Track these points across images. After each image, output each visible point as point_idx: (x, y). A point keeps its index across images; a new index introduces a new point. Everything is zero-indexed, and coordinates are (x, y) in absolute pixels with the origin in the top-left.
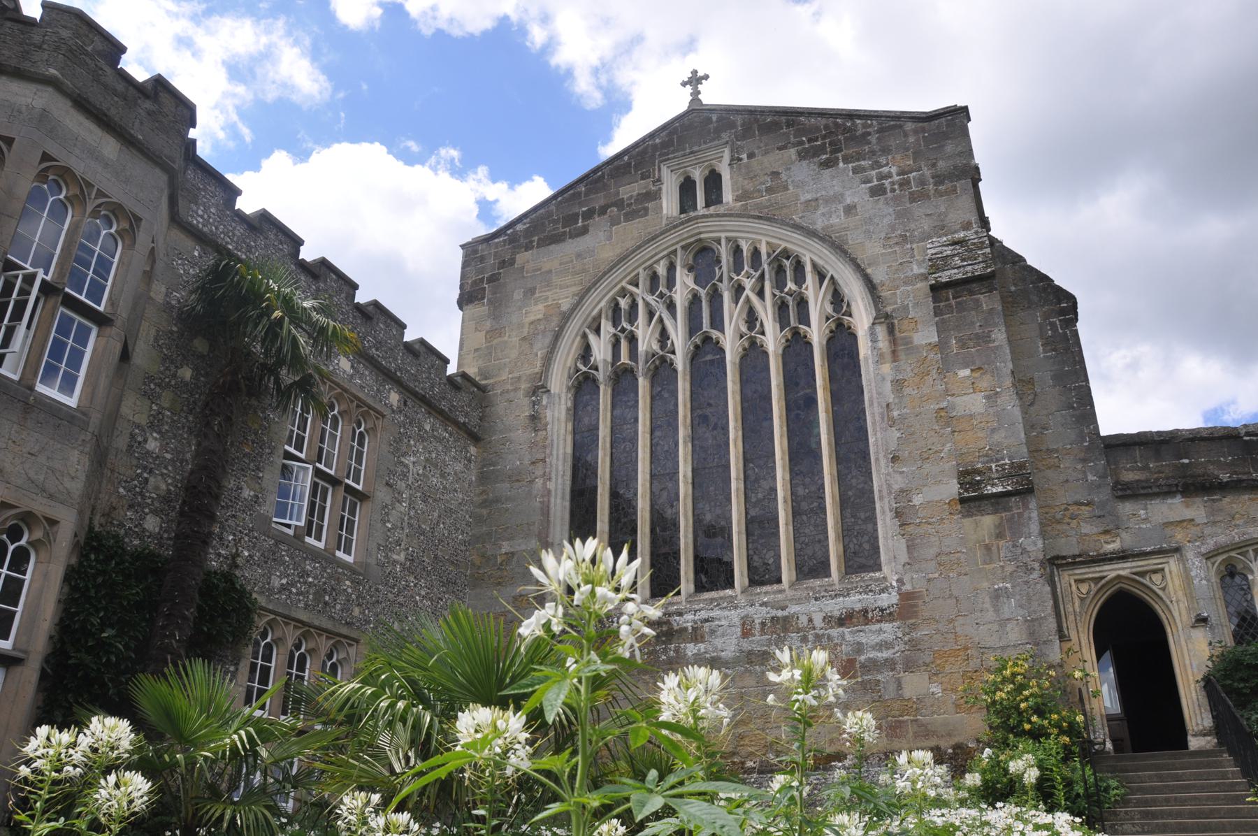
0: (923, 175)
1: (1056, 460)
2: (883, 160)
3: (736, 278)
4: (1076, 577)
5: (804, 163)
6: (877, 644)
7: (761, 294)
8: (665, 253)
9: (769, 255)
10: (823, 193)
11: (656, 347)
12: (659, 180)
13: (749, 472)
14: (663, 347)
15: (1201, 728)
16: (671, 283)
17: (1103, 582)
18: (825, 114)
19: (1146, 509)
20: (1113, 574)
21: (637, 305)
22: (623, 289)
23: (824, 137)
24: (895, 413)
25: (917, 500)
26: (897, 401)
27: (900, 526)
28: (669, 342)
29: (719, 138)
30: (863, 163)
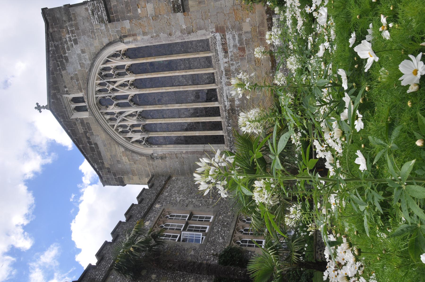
0: (69, 25)
3: (110, 91)
5: (67, 68)
6: (233, 40)
7: (115, 82)
8: (102, 116)
9: (101, 80)
10: (77, 61)
11: (135, 118)
12: (76, 119)
13: (177, 84)
14: (135, 115)
16: (112, 114)
18: (48, 61)
21: (121, 125)
22: (115, 130)
23: (57, 61)
25: (184, 27)
26: (150, 34)
27: (193, 33)
28: (133, 113)
29: (59, 99)
30: (66, 47)
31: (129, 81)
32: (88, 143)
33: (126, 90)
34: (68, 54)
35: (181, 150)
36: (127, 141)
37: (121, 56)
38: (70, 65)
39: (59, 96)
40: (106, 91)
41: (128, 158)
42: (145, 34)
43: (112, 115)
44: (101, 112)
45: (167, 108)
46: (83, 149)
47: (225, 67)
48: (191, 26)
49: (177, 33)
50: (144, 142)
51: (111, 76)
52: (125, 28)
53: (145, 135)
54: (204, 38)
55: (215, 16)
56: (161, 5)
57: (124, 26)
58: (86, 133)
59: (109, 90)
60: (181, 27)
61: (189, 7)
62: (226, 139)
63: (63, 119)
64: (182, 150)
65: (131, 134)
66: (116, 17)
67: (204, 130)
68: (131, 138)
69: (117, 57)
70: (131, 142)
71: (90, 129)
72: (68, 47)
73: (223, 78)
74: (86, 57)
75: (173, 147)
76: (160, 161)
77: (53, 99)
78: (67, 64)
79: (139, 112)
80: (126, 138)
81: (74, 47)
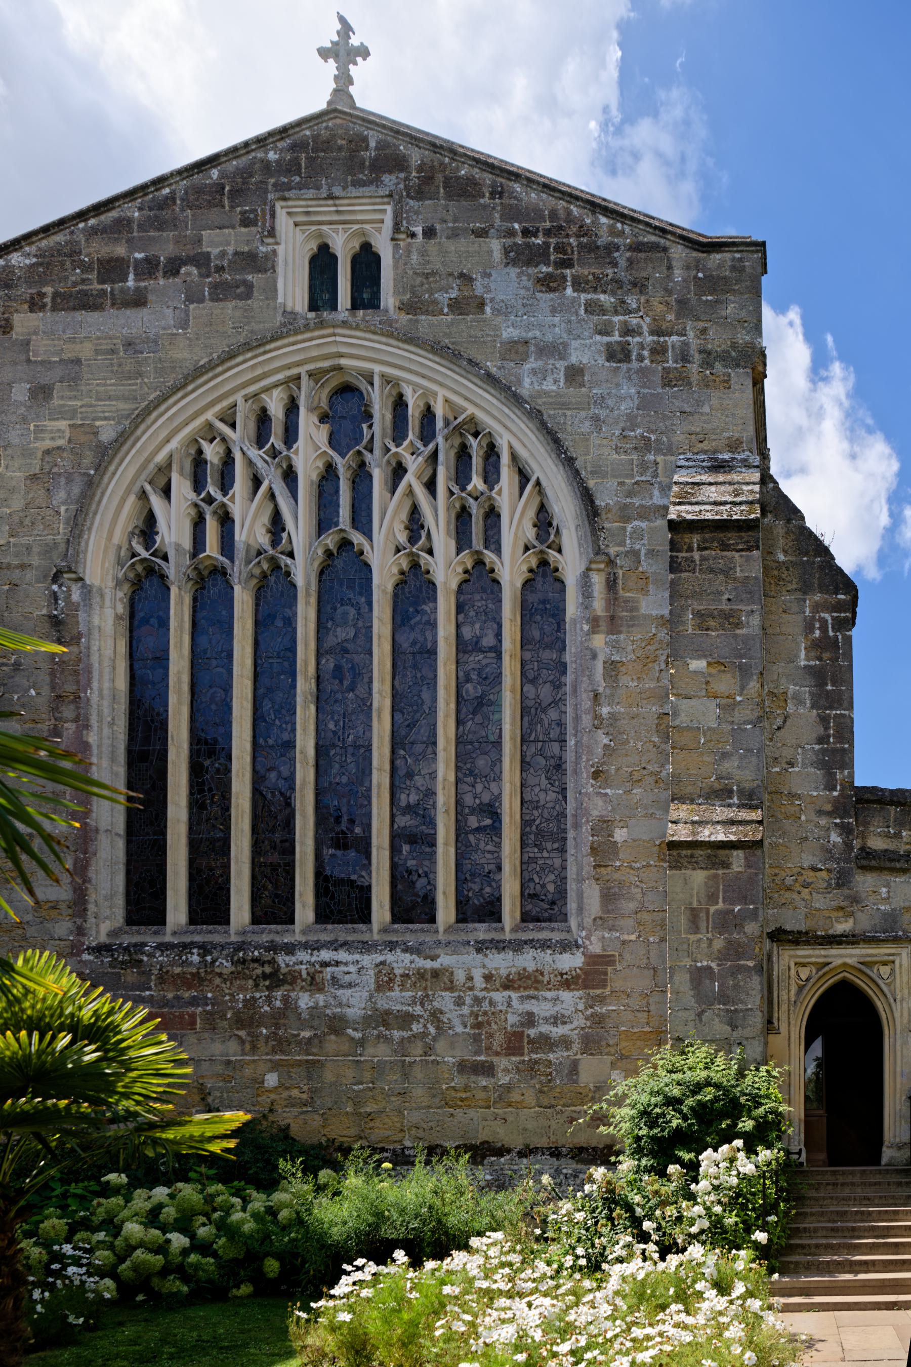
1: (797, 808)
2: (632, 301)
4: (798, 960)
5: (514, 271)
6: (552, 1016)
7: (431, 486)
8: (280, 376)
9: (447, 423)
10: (538, 333)
11: (263, 539)
12: (272, 233)
15: (898, 1140)
16: (290, 435)
17: (827, 969)
18: (554, 190)
19: (888, 886)
20: (839, 961)
21: (233, 459)
22: (210, 426)
23: (548, 233)
24: (605, 711)
25: (620, 835)
26: (608, 692)
27: (595, 867)
29: (376, 182)
30: (602, 297)
31: (430, 552)
32: (146, 260)
33: (391, 528)
34: (574, 300)
35: (100, 721)
36: (151, 466)
37: (536, 543)
38: (522, 292)
39: (389, 180)
40: (399, 431)
41: (59, 448)
42: (612, 667)
43: (287, 430)
44: (298, 377)
45: (299, 699)
46: (118, 221)
47: (452, 973)
48: (618, 864)
49: (599, 802)
50: (145, 554)
51: (462, 476)
52: (644, 591)
53: (178, 566)
54: (572, 906)
55: (645, 961)
56: (707, 759)
57: (651, 587)
58: (201, 261)
59: (399, 450)
60: (621, 824)
61: (686, 868)
62: (149, 938)
63: (277, 162)
64: (101, 729)
65: (186, 499)
66: (686, 559)
67: (193, 845)
68: (166, 492)
69: (535, 526)
70: (148, 488)
71: (221, 292)
72: (603, 311)
73: (407, 957)
74: (550, 379)
75: (114, 689)
76: (44, 612)
77: (381, 146)
78: (529, 275)
79: (286, 565)
80: (165, 469)
81: (598, 338)
